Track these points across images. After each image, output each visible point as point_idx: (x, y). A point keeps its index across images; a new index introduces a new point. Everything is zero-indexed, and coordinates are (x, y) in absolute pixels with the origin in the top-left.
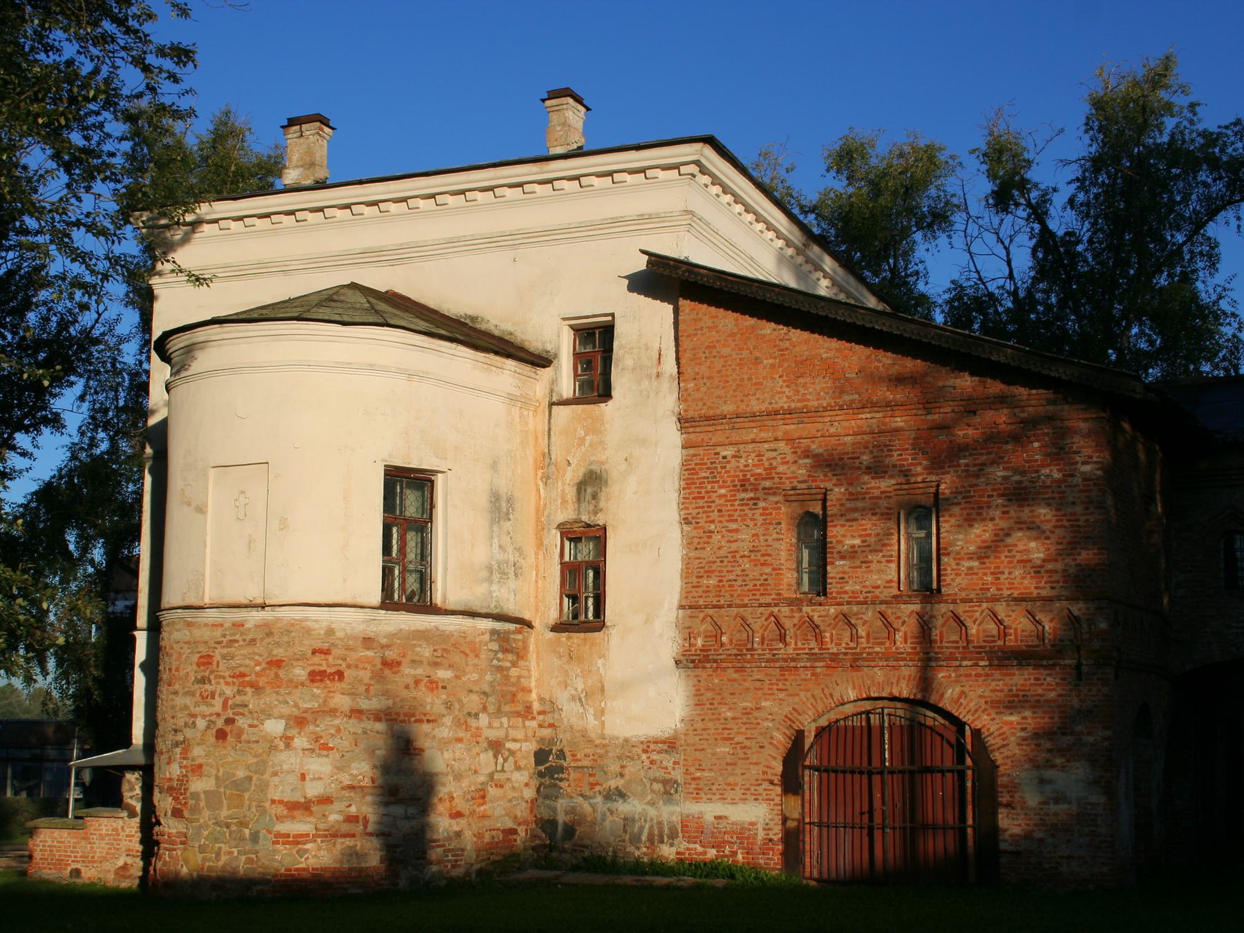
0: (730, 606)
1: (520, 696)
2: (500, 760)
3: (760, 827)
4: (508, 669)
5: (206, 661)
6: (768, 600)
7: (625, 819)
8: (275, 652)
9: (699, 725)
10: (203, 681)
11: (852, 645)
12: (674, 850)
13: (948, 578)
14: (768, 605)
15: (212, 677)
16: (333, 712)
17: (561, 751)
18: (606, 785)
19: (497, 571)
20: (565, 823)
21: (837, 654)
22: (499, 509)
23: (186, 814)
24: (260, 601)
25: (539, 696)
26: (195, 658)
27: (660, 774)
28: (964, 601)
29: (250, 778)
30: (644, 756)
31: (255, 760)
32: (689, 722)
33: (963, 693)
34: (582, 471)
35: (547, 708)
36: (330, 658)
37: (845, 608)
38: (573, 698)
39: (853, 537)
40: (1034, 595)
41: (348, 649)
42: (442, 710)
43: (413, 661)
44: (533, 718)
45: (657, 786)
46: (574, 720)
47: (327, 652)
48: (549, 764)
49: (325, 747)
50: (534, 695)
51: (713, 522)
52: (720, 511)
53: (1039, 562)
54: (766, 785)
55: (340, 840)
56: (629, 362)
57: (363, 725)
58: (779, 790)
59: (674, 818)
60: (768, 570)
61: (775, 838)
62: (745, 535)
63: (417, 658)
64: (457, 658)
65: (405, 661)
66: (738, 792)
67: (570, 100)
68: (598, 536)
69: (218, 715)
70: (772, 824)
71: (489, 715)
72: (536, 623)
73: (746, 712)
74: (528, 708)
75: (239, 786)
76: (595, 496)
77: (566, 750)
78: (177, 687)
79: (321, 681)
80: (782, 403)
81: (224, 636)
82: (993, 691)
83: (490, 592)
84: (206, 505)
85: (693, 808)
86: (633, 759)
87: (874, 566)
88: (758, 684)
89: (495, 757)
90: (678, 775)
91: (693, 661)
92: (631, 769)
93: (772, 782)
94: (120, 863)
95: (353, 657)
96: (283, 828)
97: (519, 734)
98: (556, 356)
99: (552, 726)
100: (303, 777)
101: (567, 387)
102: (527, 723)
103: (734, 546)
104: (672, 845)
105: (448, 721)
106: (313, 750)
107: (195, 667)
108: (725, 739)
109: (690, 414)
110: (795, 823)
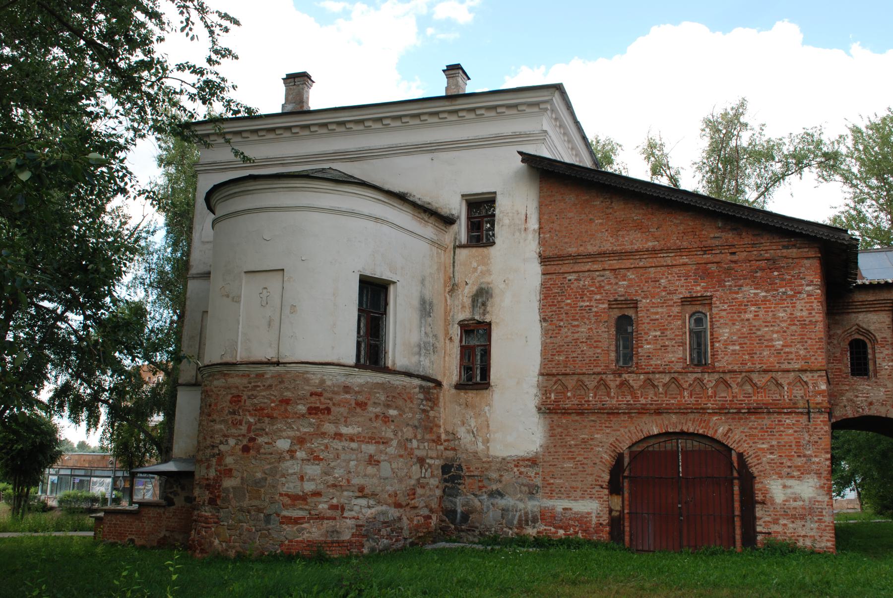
0: (574, 374)
1: (435, 429)
2: (424, 471)
3: (594, 515)
4: (428, 412)
5: (236, 399)
6: (599, 369)
7: (503, 510)
8: (285, 394)
9: (553, 450)
10: (234, 413)
11: (655, 399)
12: (535, 530)
13: (719, 357)
14: (599, 373)
15: (240, 411)
16: (323, 434)
17: (460, 465)
18: (490, 488)
19: (424, 348)
20: (462, 512)
21: (646, 405)
22: (425, 309)
23: (219, 502)
24: (275, 360)
25: (445, 430)
26: (229, 397)
27: (525, 481)
28: (730, 372)
29: (266, 479)
30: (515, 469)
31: (269, 466)
32: (546, 448)
33: (730, 430)
34: (475, 288)
35: (451, 437)
36: (322, 399)
37: (651, 376)
38: (468, 432)
39: (655, 330)
40: (777, 367)
41: (334, 393)
42: (392, 437)
43: (375, 403)
44: (442, 444)
45: (524, 489)
46: (468, 446)
47: (320, 395)
48: (452, 474)
49: (317, 458)
50: (442, 430)
51: (562, 320)
52: (566, 313)
53: (779, 347)
54: (598, 488)
55: (326, 521)
56: (506, 221)
57: (342, 444)
58: (606, 491)
59: (535, 509)
60: (599, 351)
61: (604, 523)
62: (583, 329)
63: (377, 401)
64: (400, 402)
65: (370, 403)
66: (579, 493)
67: (461, 72)
68: (485, 328)
69: (244, 436)
70: (602, 513)
71: (418, 440)
72: (445, 383)
73: (584, 441)
74: (439, 437)
75: (259, 483)
76: (484, 304)
77: (463, 465)
78: (215, 417)
79: (316, 414)
80: (607, 247)
81: (250, 383)
82: (750, 428)
83: (420, 361)
84: (240, 297)
85: (548, 503)
86: (507, 471)
87: (669, 349)
88: (592, 424)
89: (421, 468)
90: (538, 481)
91: (549, 409)
92: (507, 477)
93: (602, 487)
94: (162, 535)
95: (337, 398)
96: (285, 513)
97: (433, 454)
98: (458, 217)
99: (454, 449)
100: (302, 478)
101: (463, 238)
102: (438, 447)
103: (576, 336)
104: (534, 527)
105: (394, 443)
106: (309, 460)
107: (228, 404)
108: (569, 458)
109: (547, 254)
110: (618, 513)
